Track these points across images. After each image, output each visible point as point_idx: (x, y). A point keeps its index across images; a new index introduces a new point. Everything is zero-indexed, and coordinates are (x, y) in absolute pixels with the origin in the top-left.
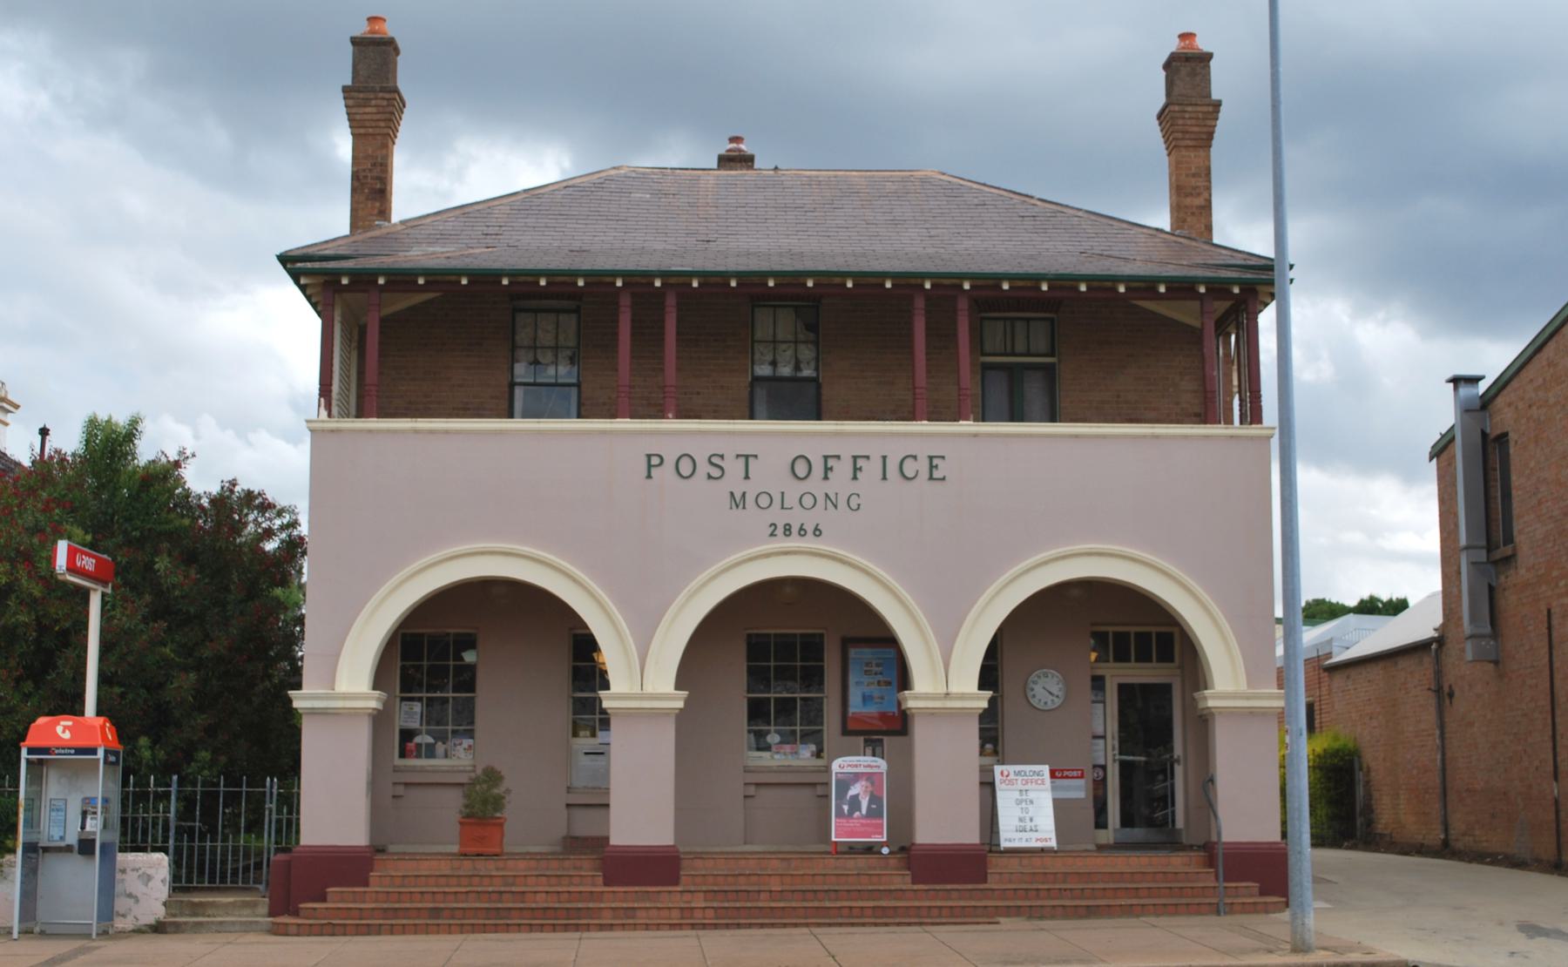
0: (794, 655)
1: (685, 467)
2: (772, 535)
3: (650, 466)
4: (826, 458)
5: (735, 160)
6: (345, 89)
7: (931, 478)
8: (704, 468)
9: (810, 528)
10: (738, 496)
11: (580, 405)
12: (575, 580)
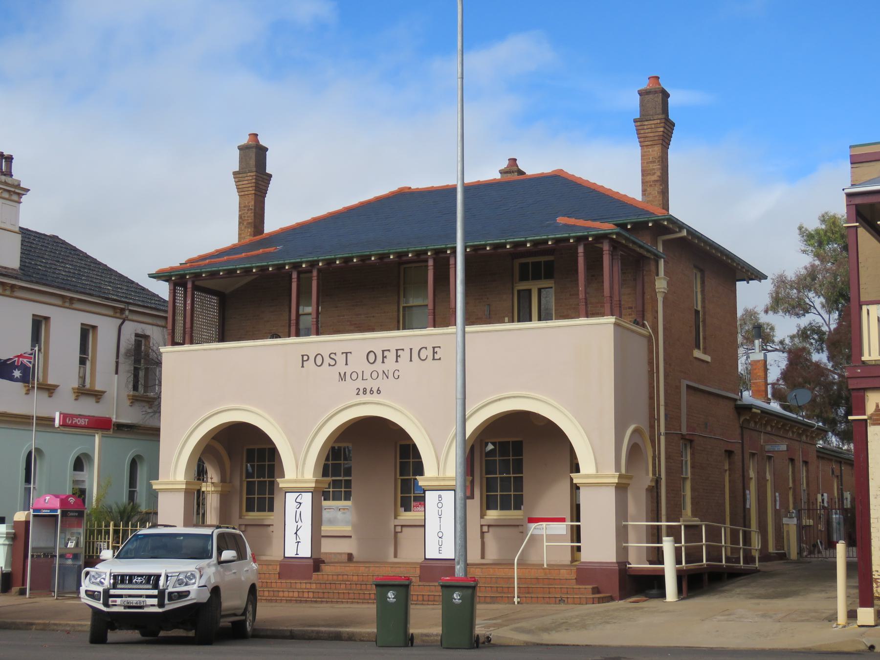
0: (372, 456)
1: (319, 360)
2: (358, 394)
3: (303, 361)
4: (383, 351)
6: (235, 173)
7: (434, 359)
8: (327, 360)
9: (375, 390)
10: (342, 375)
11: (317, 328)
12: (395, 409)
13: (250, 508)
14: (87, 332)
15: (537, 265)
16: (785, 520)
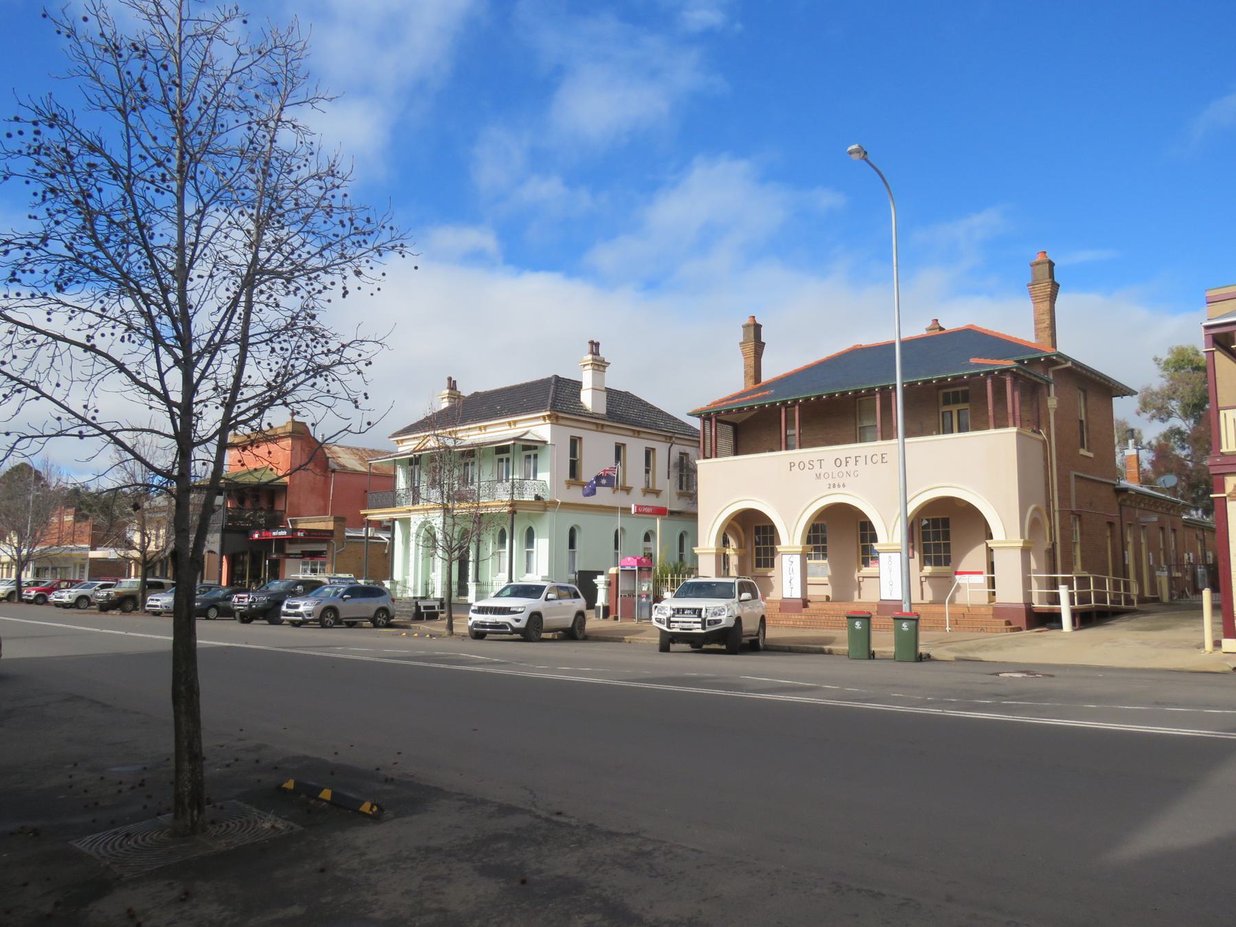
5: (145, 807)
8: (807, 466)
13: (758, 565)
14: (649, 453)
15: (956, 393)
16: (1158, 573)
